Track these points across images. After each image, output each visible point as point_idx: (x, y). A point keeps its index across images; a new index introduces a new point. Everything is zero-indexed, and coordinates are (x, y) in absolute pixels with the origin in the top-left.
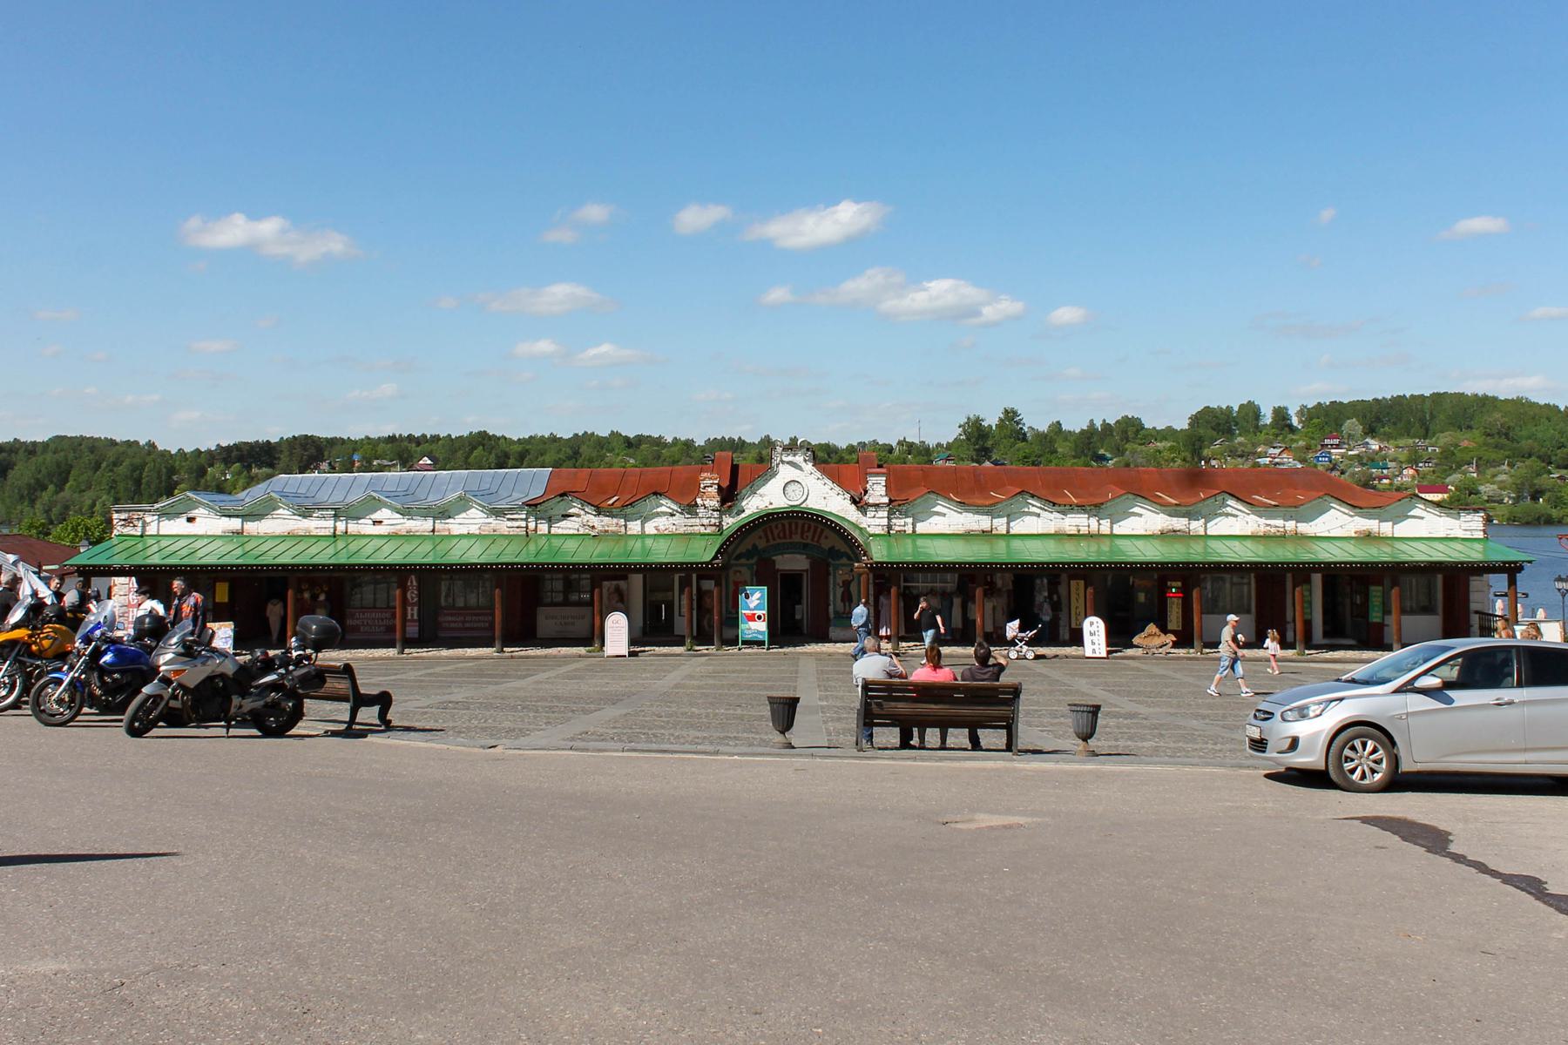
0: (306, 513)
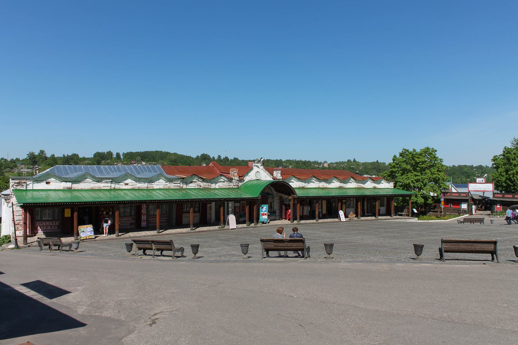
0: (99, 180)
